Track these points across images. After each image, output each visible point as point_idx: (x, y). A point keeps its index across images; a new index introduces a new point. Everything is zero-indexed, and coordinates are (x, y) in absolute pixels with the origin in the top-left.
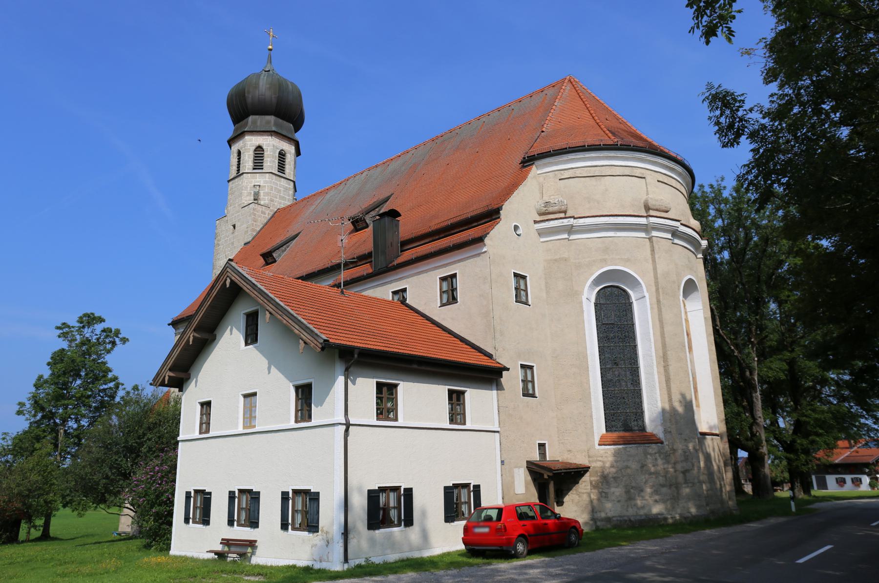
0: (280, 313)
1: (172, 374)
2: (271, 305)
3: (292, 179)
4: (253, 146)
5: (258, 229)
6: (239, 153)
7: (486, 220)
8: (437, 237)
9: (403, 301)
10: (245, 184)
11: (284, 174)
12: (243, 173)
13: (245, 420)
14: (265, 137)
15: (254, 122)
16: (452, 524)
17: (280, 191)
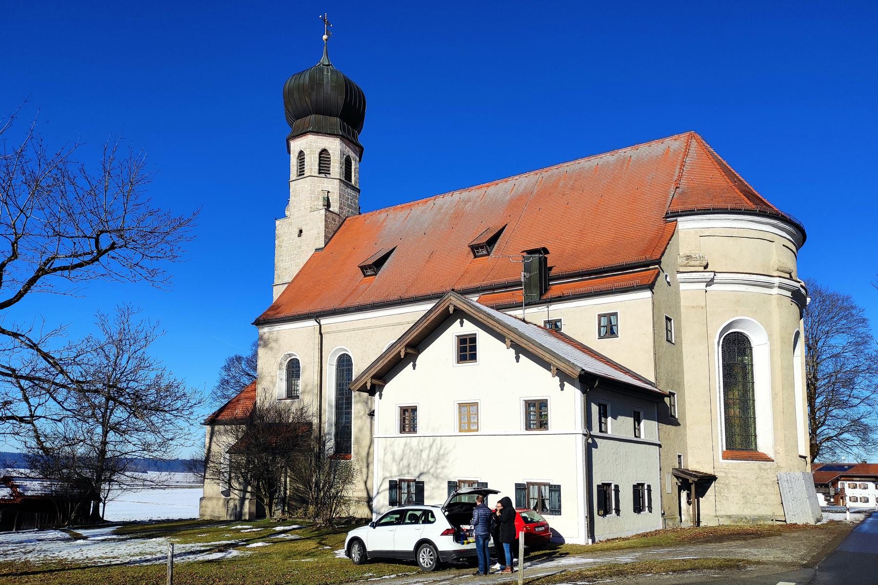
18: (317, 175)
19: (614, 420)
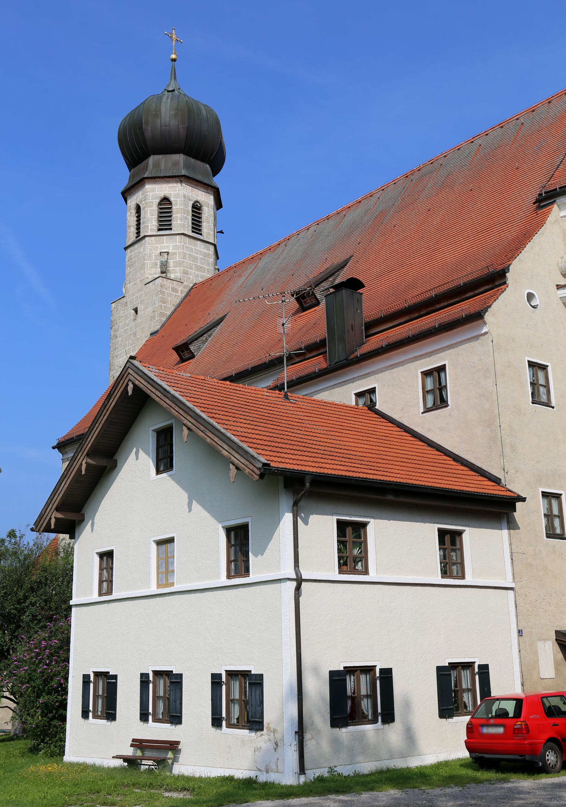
0: (203, 428)
1: (59, 516)
2: (189, 418)
3: (212, 241)
4: (157, 198)
5: (169, 313)
6: (138, 209)
7: (487, 287)
8: (417, 315)
9: (371, 406)
10: (147, 252)
11: (201, 234)
13: (160, 575)
14: (171, 185)
15: (157, 165)
16: (450, 720)
17: (196, 258)
19: (255, 558)
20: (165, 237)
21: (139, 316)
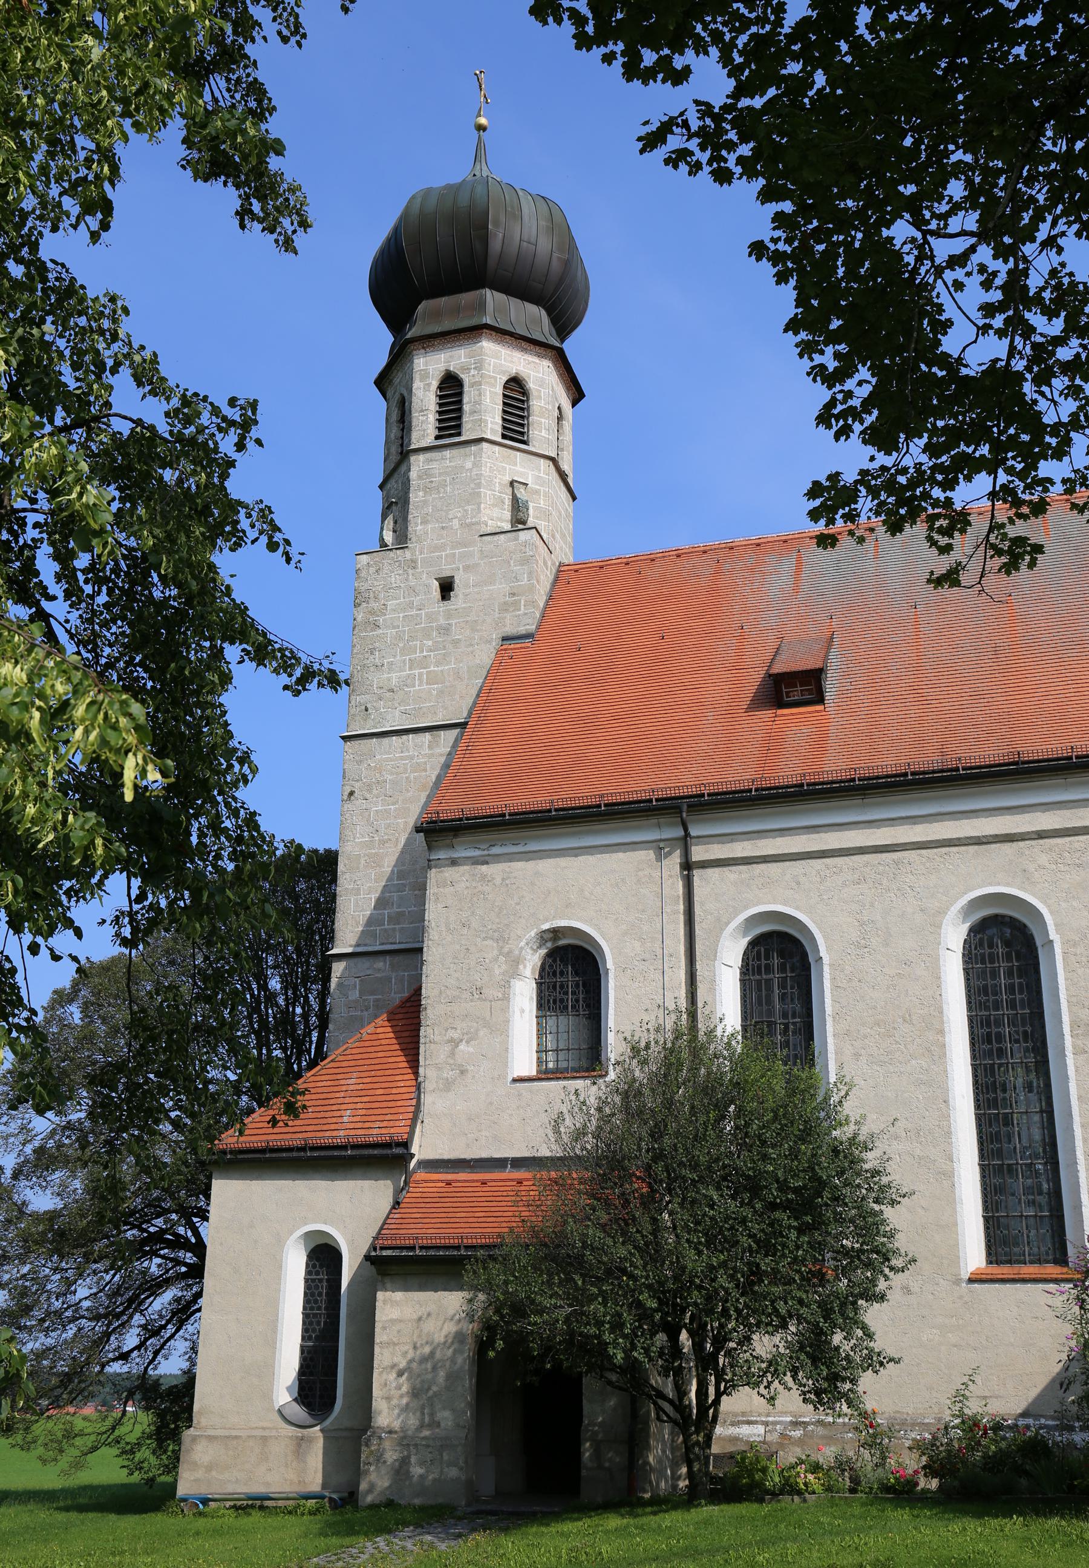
4: (504, 373)
10: (485, 471)
12: (482, 440)
18: (499, 439)
20: (518, 453)
21: (461, 596)
